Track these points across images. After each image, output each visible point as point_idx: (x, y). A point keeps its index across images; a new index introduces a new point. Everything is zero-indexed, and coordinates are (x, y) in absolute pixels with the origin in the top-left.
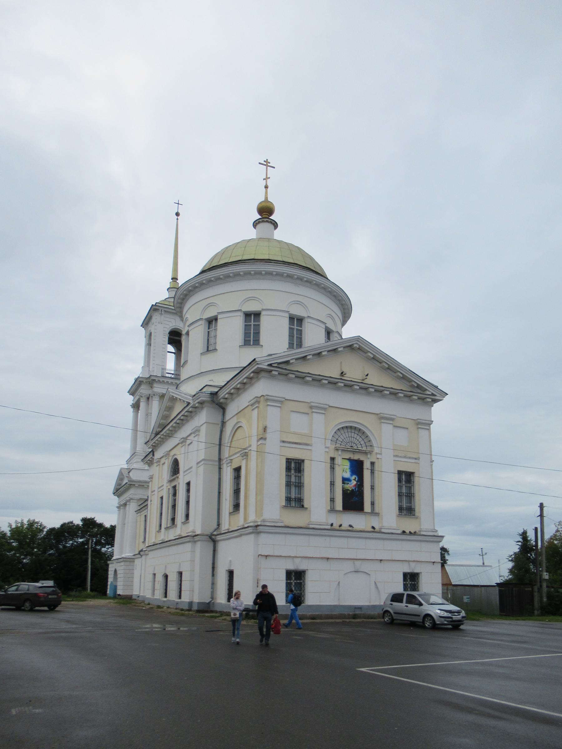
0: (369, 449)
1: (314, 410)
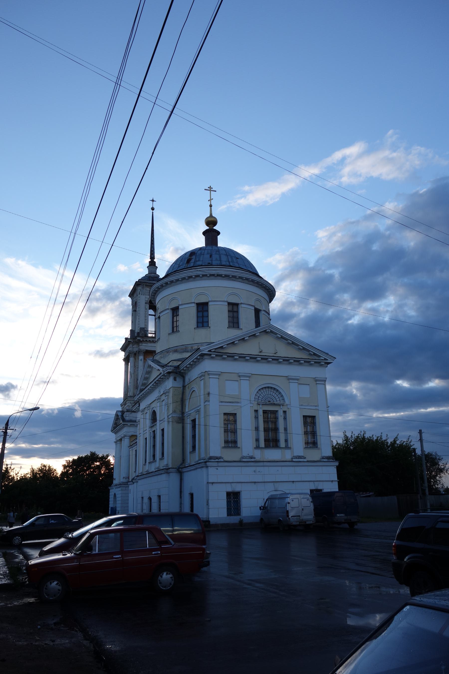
0: (282, 402)
1: (241, 378)
